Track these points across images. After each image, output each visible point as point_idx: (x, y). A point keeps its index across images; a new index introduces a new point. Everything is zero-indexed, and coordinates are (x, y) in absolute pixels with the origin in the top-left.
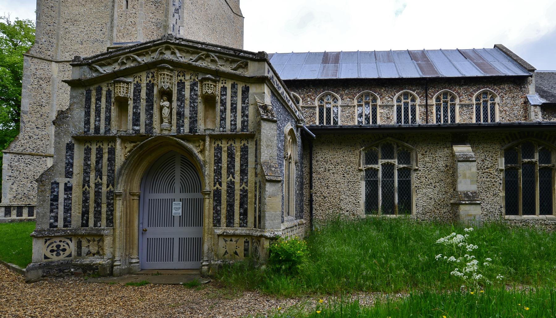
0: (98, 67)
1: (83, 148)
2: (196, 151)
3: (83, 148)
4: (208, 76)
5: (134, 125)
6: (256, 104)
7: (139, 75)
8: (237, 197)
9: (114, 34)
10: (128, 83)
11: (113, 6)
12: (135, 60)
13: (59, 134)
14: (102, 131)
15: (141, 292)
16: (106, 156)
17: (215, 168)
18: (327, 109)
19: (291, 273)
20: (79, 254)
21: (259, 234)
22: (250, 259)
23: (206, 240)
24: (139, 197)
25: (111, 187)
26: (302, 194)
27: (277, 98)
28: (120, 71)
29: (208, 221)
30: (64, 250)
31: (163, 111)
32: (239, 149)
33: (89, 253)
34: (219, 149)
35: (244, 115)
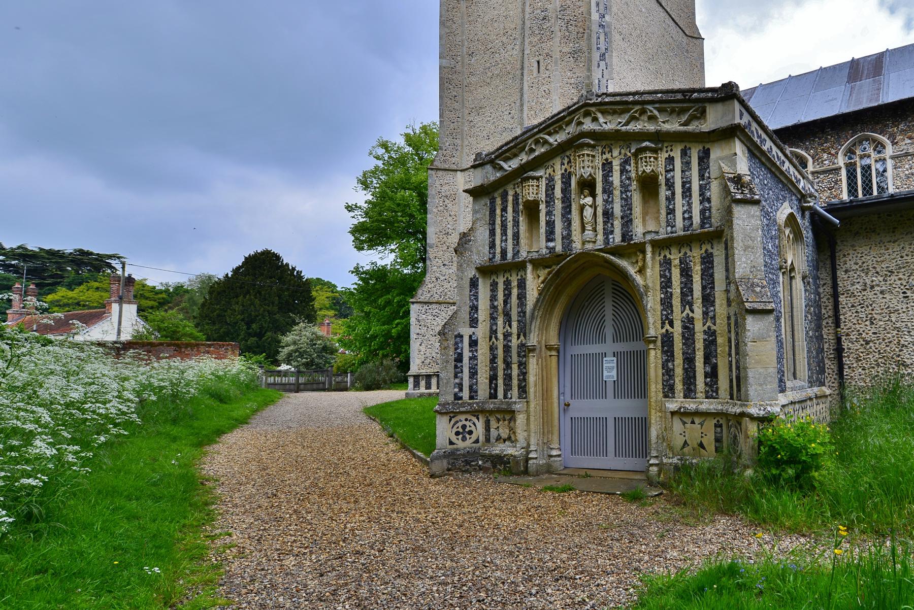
0: (502, 163)
1: (489, 282)
2: (632, 271)
3: (489, 282)
4: (644, 144)
5: (549, 240)
6: (722, 176)
7: (551, 163)
8: (699, 345)
9: (525, 116)
10: (538, 179)
11: (522, 74)
12: (546, 142)
13: (461, 266)
14: (510, 255)
15: (563, 502)
16: (515, 292)
17: (663, 296)
18: (863, 168)
19: (801, 487)
20: (488, 440)
21: (738, 411)
22: (726, 456)
23: (653, 421)
24: (558, 352)
25: (522, 337)
26: (820, 338)
27: (760, 161)
28: (528, 163)
29: (655, 388)
30: (470, 433)
31: (585, 214)
32: (698, 260)
33: (498, 438)
34: (666, 264)
35: (705, 199)
